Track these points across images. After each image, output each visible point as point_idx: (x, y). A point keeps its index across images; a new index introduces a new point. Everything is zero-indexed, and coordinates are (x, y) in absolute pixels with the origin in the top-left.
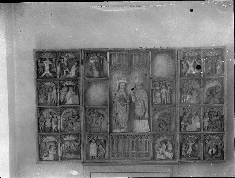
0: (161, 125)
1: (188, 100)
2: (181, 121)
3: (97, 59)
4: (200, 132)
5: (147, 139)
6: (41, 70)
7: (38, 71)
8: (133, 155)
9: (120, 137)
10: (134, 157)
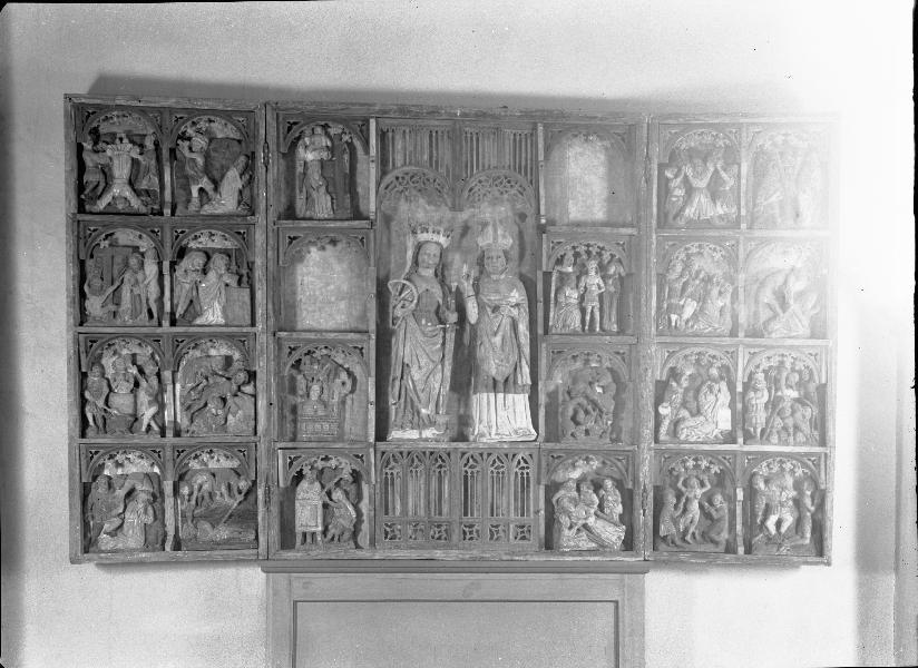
0: (581, 415)
8: (467, 529)
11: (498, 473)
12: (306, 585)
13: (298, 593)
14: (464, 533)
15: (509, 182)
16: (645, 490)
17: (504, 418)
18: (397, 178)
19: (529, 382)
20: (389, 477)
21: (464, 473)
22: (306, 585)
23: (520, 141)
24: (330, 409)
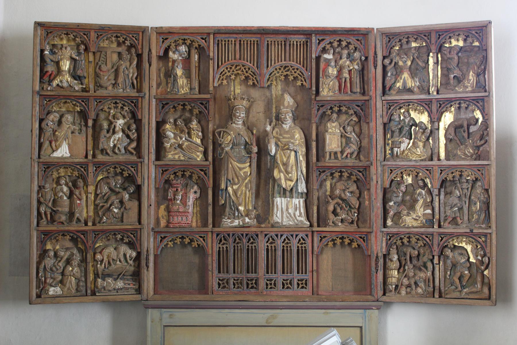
0: (338, 210)
1: (404, 151)
2: (385, 202)
3: (186, 51)
4: (431, 230)
5: (303, 245)
6: (50, 68)
7: (43, 73)
8: (268, 282)
9: (237, 239)
10: (271, 288)
11: (287, 247)
12: (171, 316)
13: (166, 321)
14: (267, 284)
15: (293, 69)
16: (377, 257)
17: (288, 211)
18: (276, 69)
19: (305, 191)
20: (250, 248)
21: (266, 247)
22: (171, 316)
23: (225, 44)
24: (187, 208)
